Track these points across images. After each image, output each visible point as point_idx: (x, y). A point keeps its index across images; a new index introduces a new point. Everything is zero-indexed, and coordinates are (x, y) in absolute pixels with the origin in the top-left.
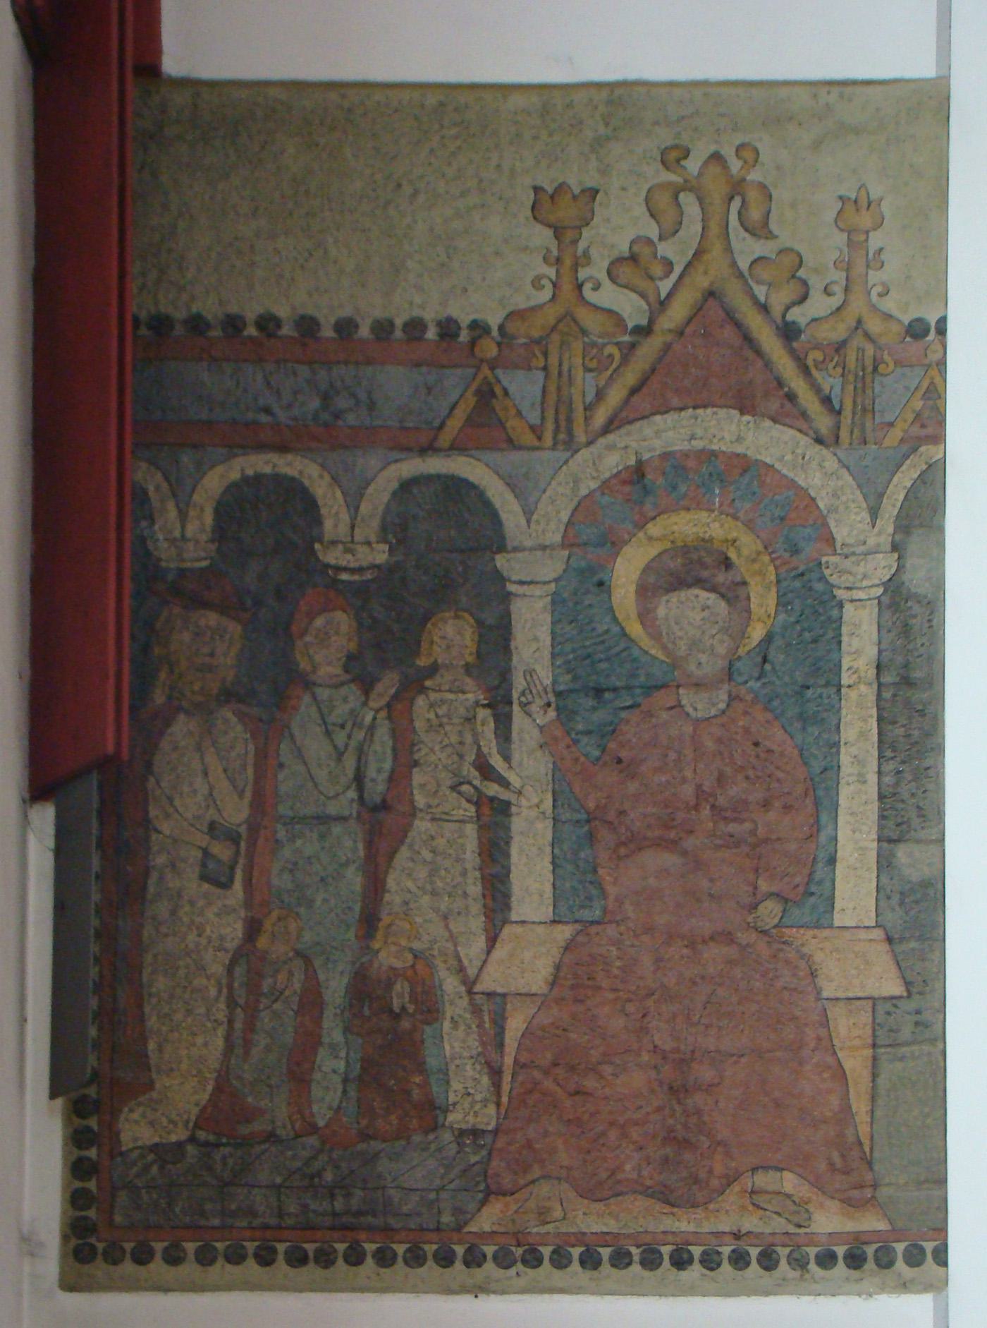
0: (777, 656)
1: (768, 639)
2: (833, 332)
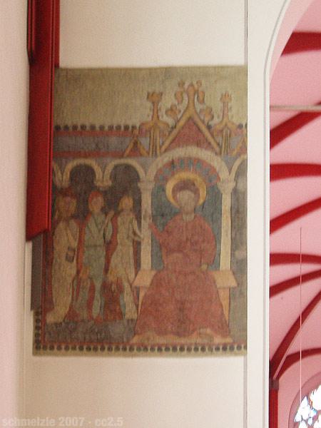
0: (206, 206)
1: (204, 203)
2: (219, 127)
